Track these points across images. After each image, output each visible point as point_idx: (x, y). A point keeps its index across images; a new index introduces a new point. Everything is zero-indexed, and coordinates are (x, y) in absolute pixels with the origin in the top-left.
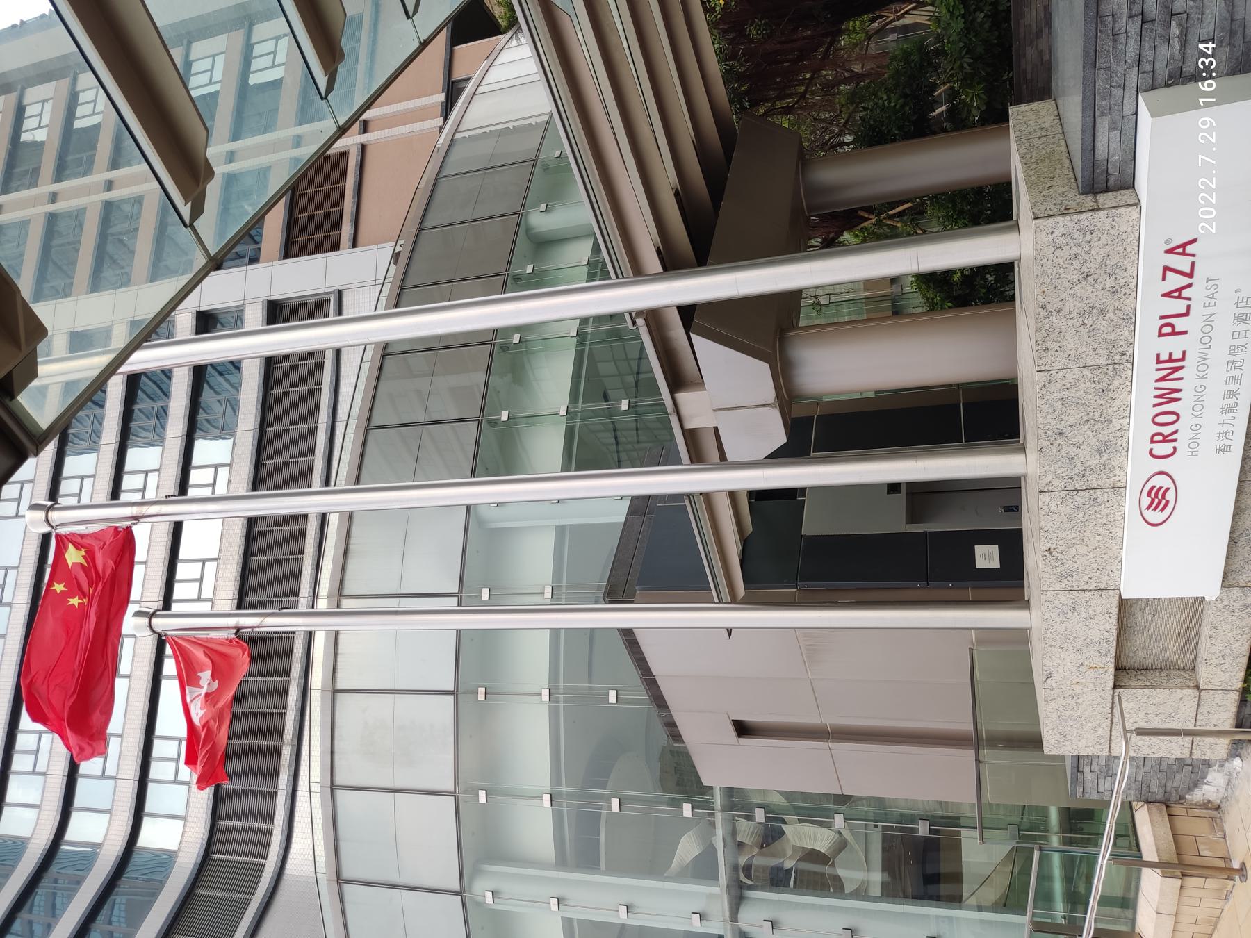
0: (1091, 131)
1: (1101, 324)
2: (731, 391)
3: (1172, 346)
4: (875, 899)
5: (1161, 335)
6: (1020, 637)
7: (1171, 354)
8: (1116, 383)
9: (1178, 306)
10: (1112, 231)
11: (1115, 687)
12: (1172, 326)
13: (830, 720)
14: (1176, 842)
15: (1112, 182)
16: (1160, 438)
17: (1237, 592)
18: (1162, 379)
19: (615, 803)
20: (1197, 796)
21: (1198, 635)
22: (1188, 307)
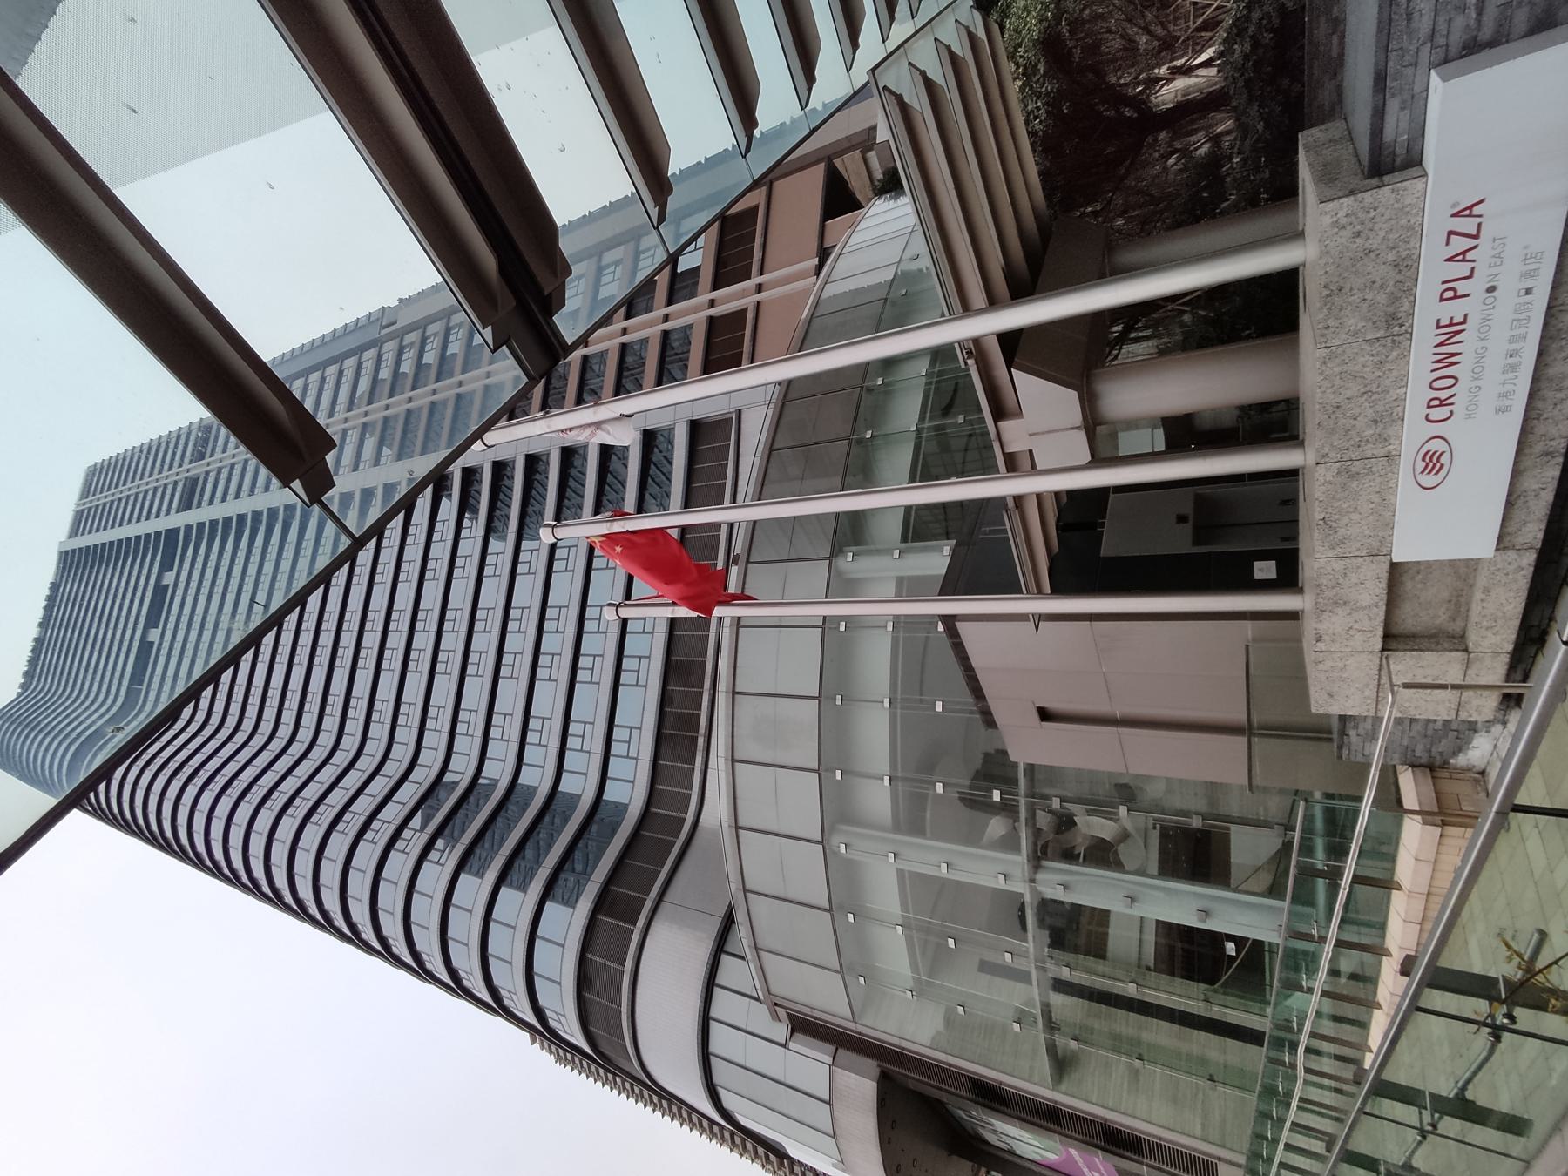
0: (1379, 114)
2: (1044, 409)
3: (1455, 309)
4: (1152, 877)
9: (1462, 269)
11: (1383, 650)
12: (1454, 289)
13: (1118, 711)
14: (1438, 799)
15: (1398, 161)
17: (1511, 555)
18: (1441, 344)
19: (939, 787)
20: (1461, 760)
21: (1468, 604)
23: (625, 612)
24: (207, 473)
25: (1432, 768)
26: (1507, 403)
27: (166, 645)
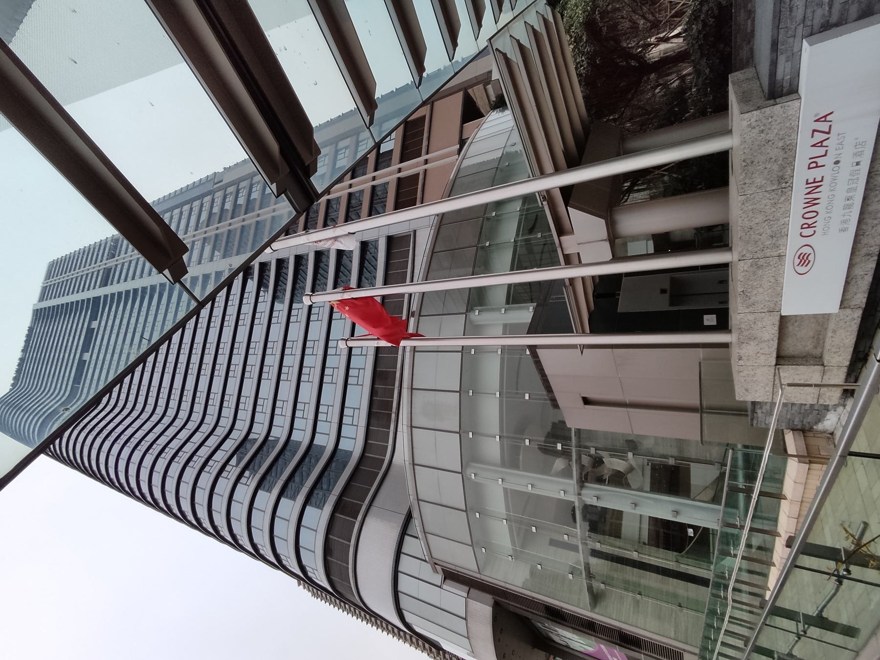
0: (774, 64)
2: (586, 230)
3: (816, 174)
4: (647, 492)
9: (821, 151)
11: (776, 365)
12: (816, 162)
13: (628, 399)
14: (807, 448)
15: (785, 90)
17: (848, 311)
18: (809, 193)
19: (527, 442)
20: (820, 427)
21: (824, 339)
24: (116, 265)
26: (846, 226)
27: (93, 362)
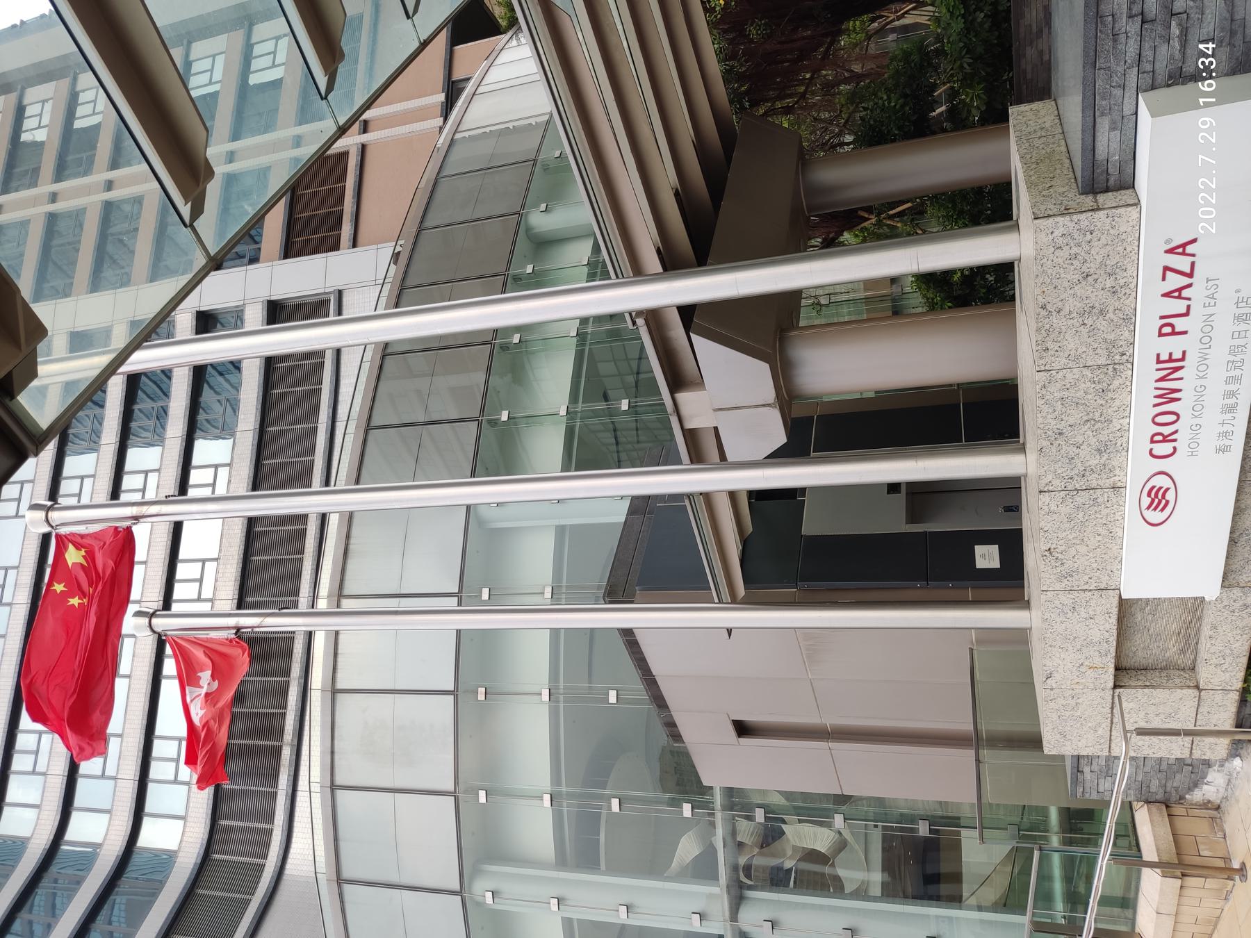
0: (1091, 131)
1: (1101, 324)
2: (731, 391)
3: (1172, 346)
4: (875, 899)
5: (1161, 335)
6: (1020, 637)
7: (1171, 354)
8: (1116, 383)
9: (1178, 306)
10: (1112, 231)
11: (1115, 687)
12: (1172, 326)
13: (830, 720)
14: (1176, 842)
15: (1112, 182)
16: (1160, 438)
17: (1237, 592)
18: (1162, 379)
19: (615, 803)
20: (1197, 796)
21: (1198, 635)
22: (1188, 307)
23: (160, 623)
25: (1167, 804)
